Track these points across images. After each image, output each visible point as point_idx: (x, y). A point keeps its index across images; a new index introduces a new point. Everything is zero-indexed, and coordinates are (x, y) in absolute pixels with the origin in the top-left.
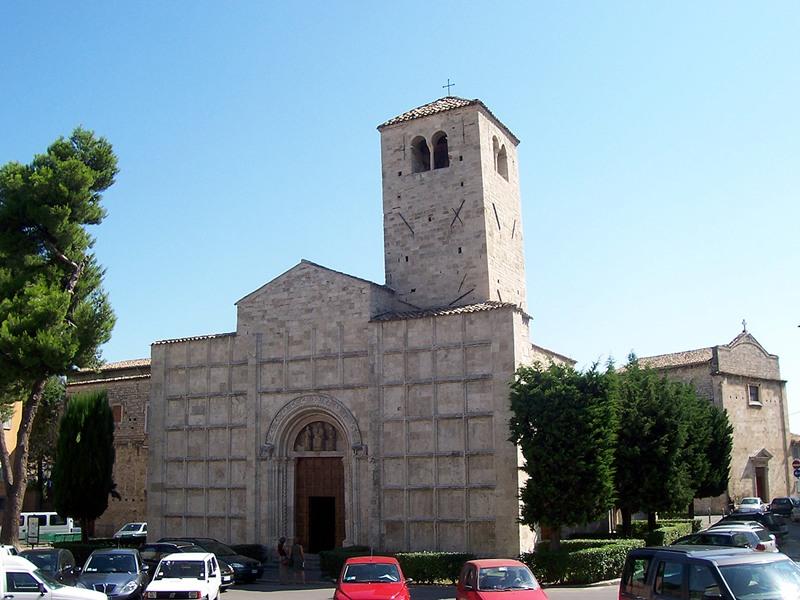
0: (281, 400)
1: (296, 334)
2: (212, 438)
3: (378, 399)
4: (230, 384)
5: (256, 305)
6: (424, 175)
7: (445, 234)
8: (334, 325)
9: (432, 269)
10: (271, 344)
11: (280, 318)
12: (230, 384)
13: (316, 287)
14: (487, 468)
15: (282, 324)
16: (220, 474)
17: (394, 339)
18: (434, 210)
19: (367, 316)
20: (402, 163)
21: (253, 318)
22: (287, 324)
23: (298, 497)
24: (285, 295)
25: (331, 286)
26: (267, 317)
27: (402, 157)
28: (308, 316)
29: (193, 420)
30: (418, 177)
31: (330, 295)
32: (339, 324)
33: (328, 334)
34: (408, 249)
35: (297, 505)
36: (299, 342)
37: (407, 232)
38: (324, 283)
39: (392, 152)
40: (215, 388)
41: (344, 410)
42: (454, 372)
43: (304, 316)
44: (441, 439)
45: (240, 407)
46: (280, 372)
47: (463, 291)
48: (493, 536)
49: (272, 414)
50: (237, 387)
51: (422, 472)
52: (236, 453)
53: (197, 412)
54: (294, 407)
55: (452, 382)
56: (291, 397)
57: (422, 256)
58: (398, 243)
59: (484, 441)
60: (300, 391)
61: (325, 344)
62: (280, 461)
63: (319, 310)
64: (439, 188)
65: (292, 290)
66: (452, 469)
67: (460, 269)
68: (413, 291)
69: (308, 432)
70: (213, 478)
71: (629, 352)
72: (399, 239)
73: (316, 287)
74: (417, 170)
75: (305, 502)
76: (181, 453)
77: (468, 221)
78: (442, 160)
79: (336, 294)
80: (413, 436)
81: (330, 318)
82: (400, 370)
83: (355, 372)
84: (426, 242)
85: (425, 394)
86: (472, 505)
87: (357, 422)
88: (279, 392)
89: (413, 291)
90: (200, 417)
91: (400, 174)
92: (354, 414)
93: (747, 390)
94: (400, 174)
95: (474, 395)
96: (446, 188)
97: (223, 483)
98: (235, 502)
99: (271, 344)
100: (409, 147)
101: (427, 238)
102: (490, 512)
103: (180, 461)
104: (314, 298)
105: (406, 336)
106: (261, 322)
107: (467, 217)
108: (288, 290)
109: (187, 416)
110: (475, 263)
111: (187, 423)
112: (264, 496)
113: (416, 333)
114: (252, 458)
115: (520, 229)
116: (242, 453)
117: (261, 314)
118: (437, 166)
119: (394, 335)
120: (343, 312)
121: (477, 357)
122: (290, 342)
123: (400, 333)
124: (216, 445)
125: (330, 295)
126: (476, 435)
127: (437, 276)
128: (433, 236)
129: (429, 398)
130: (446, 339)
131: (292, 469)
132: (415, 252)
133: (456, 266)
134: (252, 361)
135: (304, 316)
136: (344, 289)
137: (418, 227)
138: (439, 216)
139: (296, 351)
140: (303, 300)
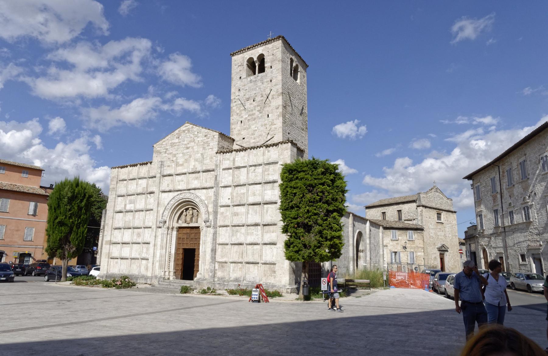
0: (171, 195)
1: (181, 161)
2: (137, 216)
3: (217, 195)
4: (147, 187)
5: (163, 146)
6: (252, 77)
7: (261, 108)
8: (200, 155)
9: (253, 127)
10: (168, 166)
11: (174, 153)
12: (147, 187)
13: (192, 136)
14: (273, 232)
15: (175, 156)
16: (139, 235)
17: (228, 162)
18: (256, 96)
19: (216, 150)
20: (241, 73)
21: (160, 153)
22: (177, 156)
23: (177, 249)
24: (177, 141)
25: (199, 135)
26: (167, 152)
27: (242, 69)
28: (188, 150)
29: (129, 207)
30: (249, 79)
31: (199, 139)
32: (202, 154)
33: (196, 160)
34: (242, 117)
35: (176, 254)
36: (182, 165)
37: (242, 108)
38: (196, 133)
39: (237, 66)
40: (140, 190)
41: (201, 201)
42: (258, 179)
43: (185, 151)
44: (249, 216)
45: (151, 199)
46: (172, 180)
47: (269, 137)
48: (275, 272)
49: (166, 203)
50: (150, 190)
51: (239, 234)
52: (147, 224)
53: (131, 203)
54: (177, 198)
55: (256, 184)
56: (176, 193)
57: (249, 120)
58: (237, 114)
59: (272, 217)
60: (181, 190)
61: (194, 166)
62: (168, 228)
63: (193, 148)
64: (259, 84)
65: (180, 137)
66: (255, 233)
67: (268, 126)
68: (244, 139)
69: (184, 213)
70: (135, 237)
71: (425, 228)
72: (238, 112)
73: (192, 136)
74: (249, 75)
75: (181, 251)
76: (120, 225)
77: (272, 101)
78: (262, 69)
79: (201, 139)
80: (236, 214)
81: (197, 151)
82: (231, 178)
83: (207, 180)
84: (251, 113)
85: (242, 191)
86: (264, 254)
87: (207, 207)
88: (170, 191)
89: (244, 139)
90: (132, 205)
91: (240, 78)
92: (206, 202)
93: (508, 269)
94: (240, 78)
95: (268, 191)
96: (263, 83)
97: (140, 240)
98: (145, 250)
99: (168, 166)
100: (245, 63)
101: (252, 111)
102: (274, 257)
103: (120, 229)
104: (191, 141)
105: (234, 160)
106: (165, 155)
107: (273, 98)
108: (179, 138)
109: (125, 205)
110: (275, 123)
111: (125, 209)
112: (159, 247)
113: (240, 158)
114: (154, 227)
115: (306, 111)
116: (150, 224)
117: (165, 150)
118: (259, 72)
119: (228, 159)
120: (204, 148)
121: (270, 170)
122: (177, 164)
123: (232, 159)
124: (138, 220)
125: (199, 139)
126: (268, 214)
127: (256, 130)
128: (255, 109)
129: (244, 193)
130: (255, 161)
131: (175, 233)
132: (246, 118)
133: (265, 125)
134: (158, 175)
135: (185, 151)
136: (206, 136)
137: (248, 105)
138: (258, 99)
139: (180, 170)
140: (185, 142)
